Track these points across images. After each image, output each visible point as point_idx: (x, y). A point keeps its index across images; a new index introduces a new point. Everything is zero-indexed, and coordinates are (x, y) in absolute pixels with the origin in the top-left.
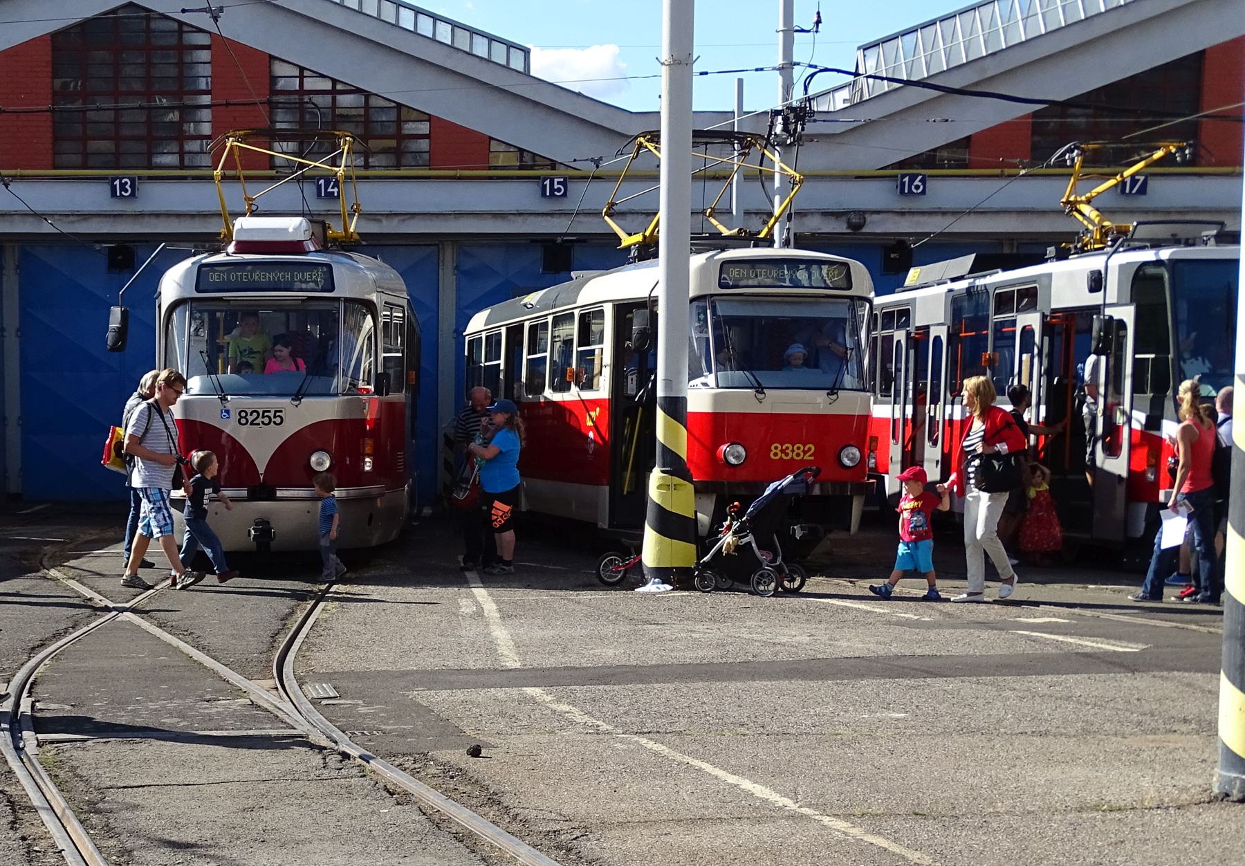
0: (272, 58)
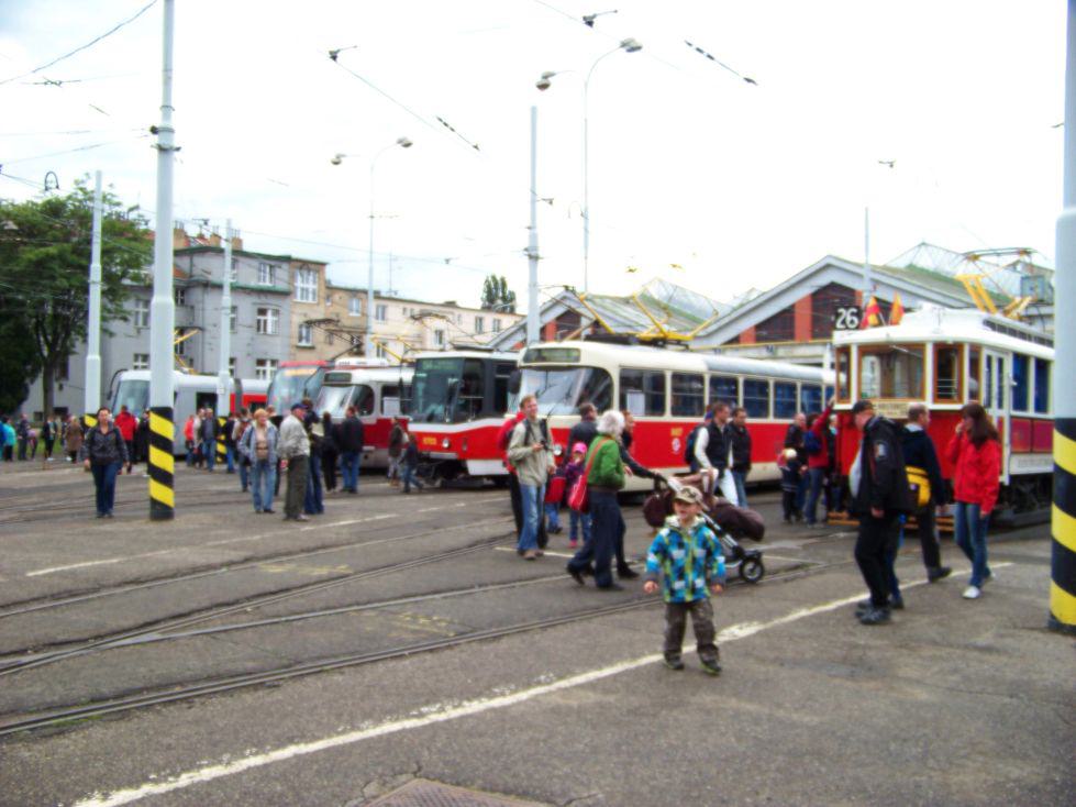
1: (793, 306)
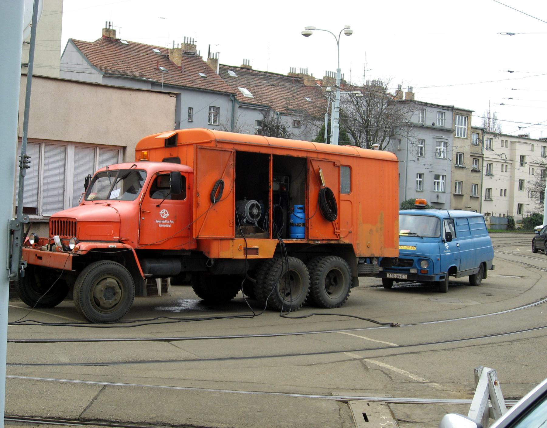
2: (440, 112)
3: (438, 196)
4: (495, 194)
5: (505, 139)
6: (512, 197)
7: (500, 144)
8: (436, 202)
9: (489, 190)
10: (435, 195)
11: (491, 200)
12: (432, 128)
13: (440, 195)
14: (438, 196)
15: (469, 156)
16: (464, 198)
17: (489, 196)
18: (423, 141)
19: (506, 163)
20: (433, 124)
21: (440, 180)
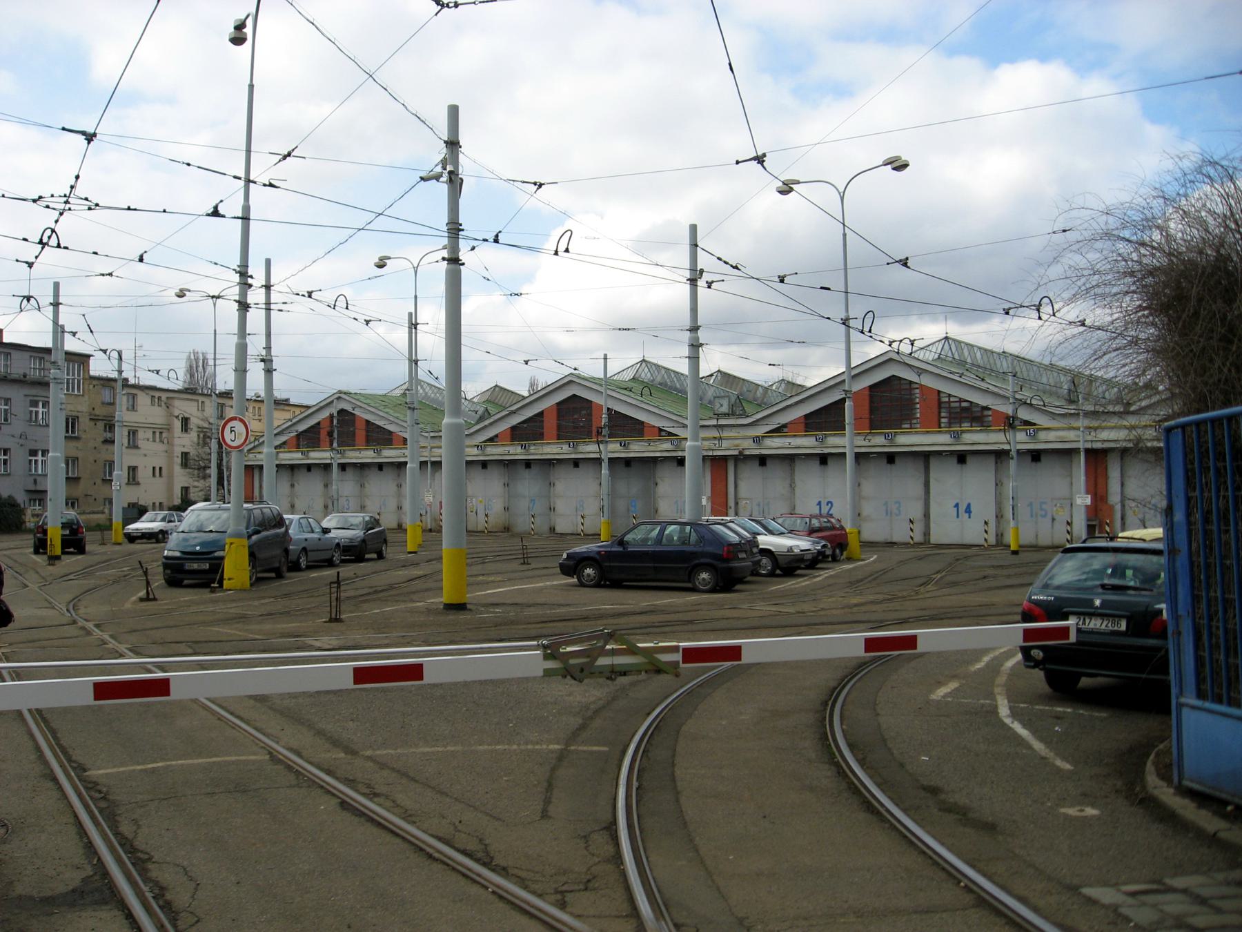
0: (939, 392)
1: (319, 423)
2: (35, 358)
3: (35, 481)
4: (144, 474)
5: (157, 394)
6: (171, 476)
7: (148, 400)
8: (33, 488)
9: (133, 470)
10: (32, 479)
11: (138, 484)
12: (22, 381)
13: (39, 479)
14: (35, 481)
15: (87, 420)
16: (82, 481)
17: (134, 479)
18: (7, 401)
19: (161, 433)
20: (25, 376)
21: (40, 458)
